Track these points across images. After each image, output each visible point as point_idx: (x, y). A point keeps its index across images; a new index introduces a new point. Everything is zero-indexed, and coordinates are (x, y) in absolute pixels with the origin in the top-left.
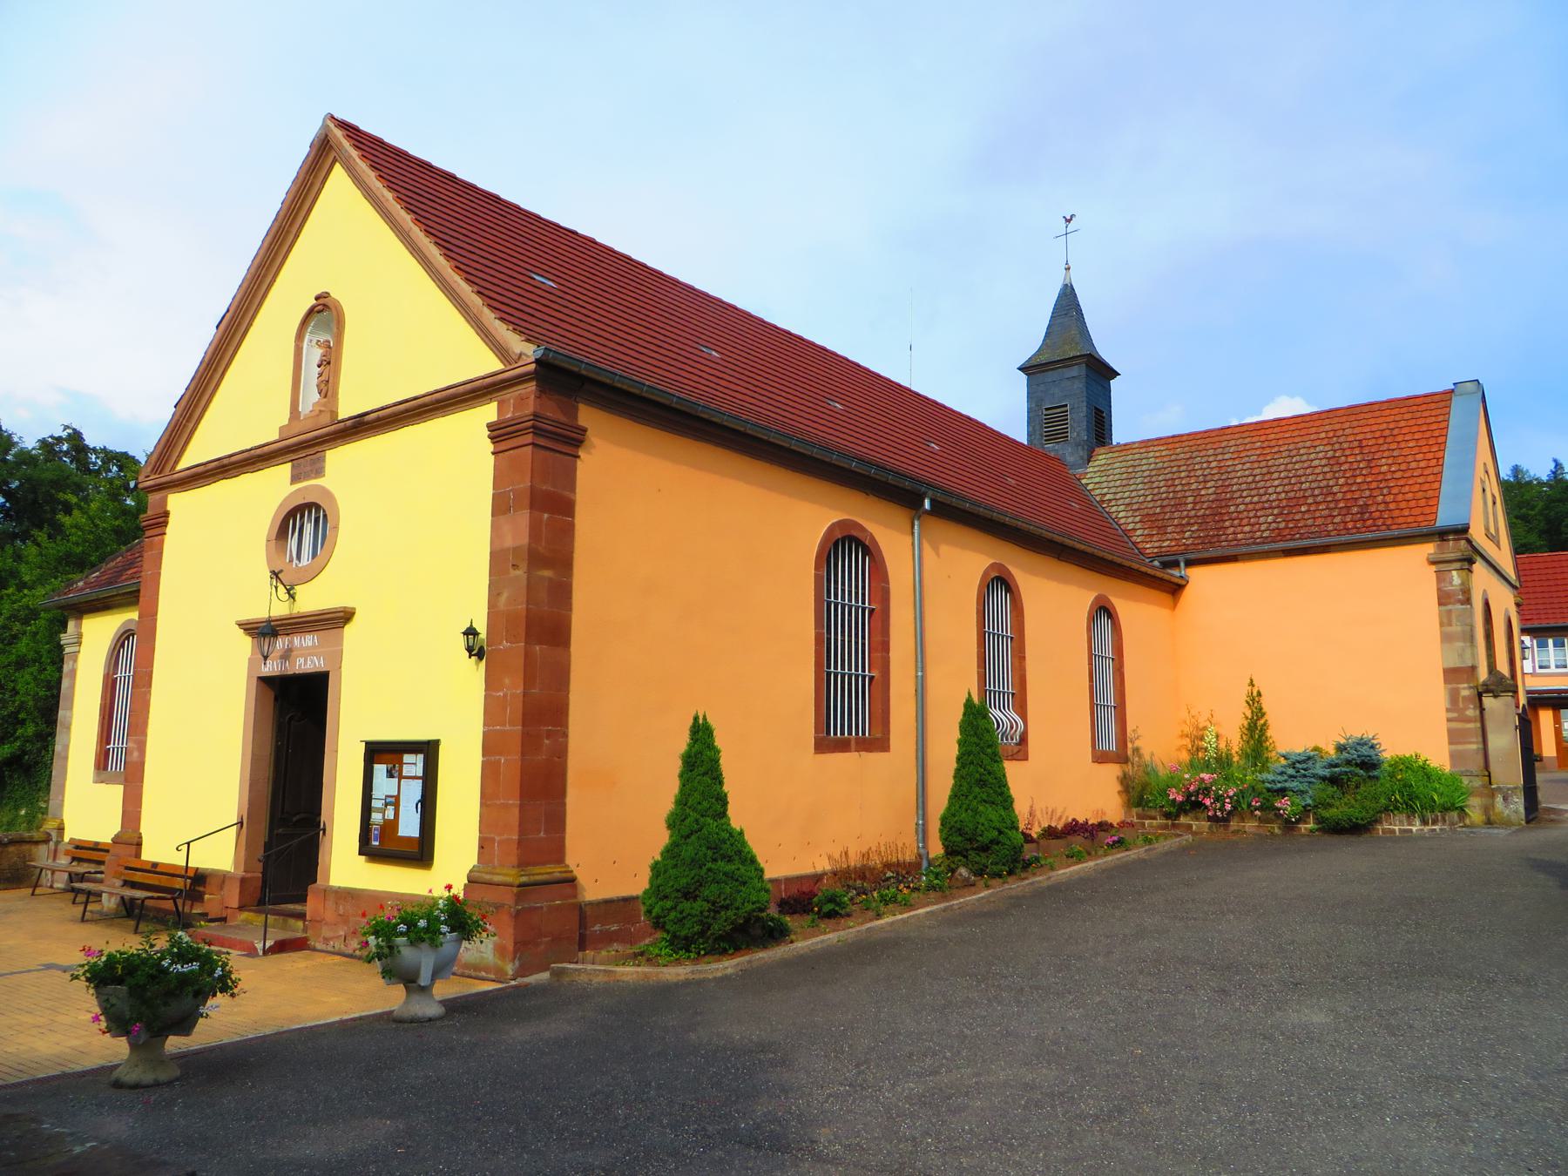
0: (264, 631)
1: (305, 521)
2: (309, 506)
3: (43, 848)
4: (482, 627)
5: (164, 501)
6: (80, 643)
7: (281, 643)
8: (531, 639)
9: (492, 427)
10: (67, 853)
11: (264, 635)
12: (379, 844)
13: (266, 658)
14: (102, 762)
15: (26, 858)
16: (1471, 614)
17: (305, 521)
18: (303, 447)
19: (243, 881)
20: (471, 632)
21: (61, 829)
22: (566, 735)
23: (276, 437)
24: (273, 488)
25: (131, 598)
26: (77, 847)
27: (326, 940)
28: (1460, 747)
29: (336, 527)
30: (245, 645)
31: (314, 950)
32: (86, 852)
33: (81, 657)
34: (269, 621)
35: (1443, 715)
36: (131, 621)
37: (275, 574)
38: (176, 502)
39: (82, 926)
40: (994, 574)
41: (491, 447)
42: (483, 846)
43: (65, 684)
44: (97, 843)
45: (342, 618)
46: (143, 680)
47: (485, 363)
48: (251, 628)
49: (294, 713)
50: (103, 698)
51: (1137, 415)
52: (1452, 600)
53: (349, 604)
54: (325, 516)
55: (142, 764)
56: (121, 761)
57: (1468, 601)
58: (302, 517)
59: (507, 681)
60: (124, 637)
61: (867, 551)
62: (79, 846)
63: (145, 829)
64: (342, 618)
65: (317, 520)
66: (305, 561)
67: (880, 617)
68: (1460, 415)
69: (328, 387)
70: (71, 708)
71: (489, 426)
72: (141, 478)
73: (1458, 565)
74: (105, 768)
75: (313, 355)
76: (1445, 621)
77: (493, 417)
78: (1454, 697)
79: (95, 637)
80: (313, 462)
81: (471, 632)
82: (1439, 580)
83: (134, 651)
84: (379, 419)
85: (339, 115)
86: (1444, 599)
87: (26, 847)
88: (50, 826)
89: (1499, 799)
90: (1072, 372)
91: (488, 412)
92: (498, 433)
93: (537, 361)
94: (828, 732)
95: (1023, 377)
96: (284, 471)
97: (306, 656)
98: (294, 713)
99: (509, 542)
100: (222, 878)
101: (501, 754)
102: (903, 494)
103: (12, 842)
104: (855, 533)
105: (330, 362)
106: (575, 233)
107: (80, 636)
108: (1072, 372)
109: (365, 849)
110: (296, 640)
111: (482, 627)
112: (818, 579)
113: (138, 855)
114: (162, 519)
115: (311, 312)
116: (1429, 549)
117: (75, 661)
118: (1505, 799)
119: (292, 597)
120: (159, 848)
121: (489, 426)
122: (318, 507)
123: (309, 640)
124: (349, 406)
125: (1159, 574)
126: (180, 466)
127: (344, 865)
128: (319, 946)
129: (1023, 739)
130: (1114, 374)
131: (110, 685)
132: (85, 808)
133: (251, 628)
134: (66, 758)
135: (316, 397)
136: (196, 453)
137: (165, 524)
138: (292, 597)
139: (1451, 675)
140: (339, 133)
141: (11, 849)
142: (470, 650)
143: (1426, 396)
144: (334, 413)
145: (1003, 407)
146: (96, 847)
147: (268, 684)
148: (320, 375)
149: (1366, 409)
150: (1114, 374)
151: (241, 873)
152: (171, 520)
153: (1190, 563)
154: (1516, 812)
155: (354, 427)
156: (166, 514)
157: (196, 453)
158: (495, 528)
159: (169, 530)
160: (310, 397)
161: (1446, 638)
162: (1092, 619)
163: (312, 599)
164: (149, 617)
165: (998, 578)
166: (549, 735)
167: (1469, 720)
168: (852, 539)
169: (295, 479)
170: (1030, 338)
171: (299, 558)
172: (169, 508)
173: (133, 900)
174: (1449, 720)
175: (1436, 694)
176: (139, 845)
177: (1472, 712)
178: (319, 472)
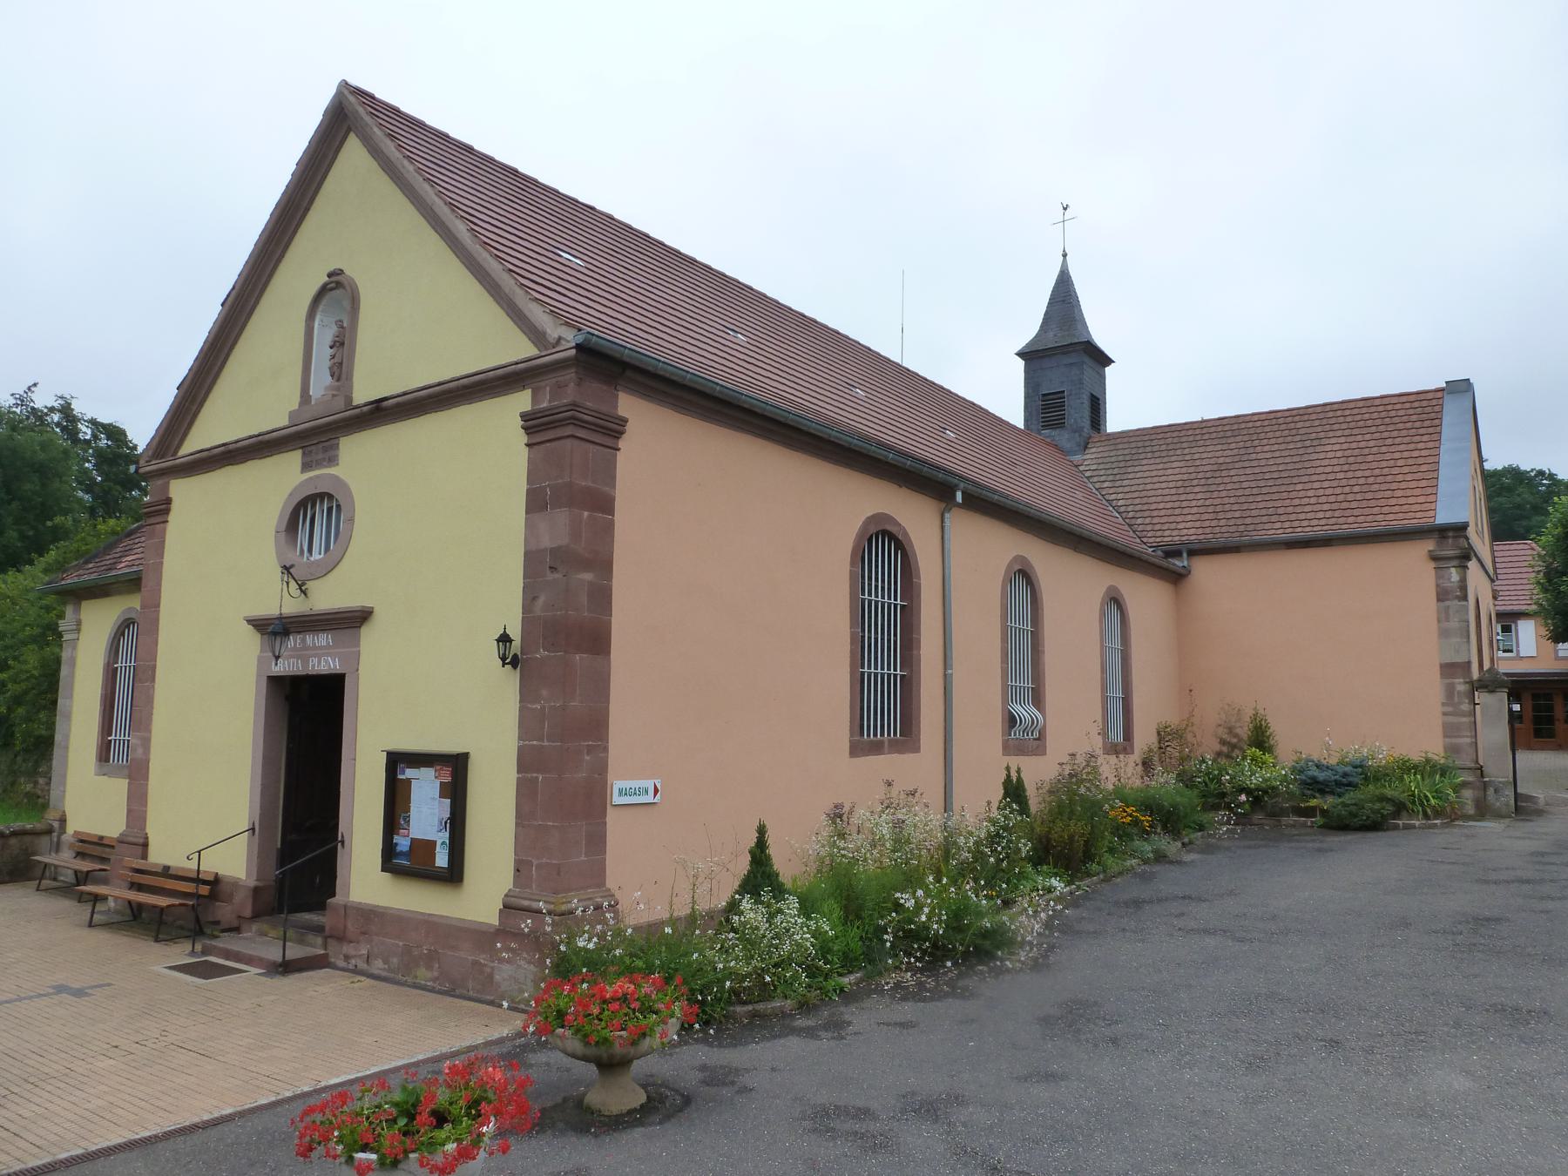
0: (275, 629)
1: (314, 513)
2: (321, 496)
3: (44, 841)
4: (515, 633)
5: (166, 488)
6: (79, 630)
7: (293, 641)
8: (562, 643)
9: (525, 417)
10: (71, 846)
11: (275, 634)
12: (405, 862)
13: (277, 658)
14: (104, 753)
15: (28, 853)
16: (1466, 608)
17: (314, 513)
18: (314, 437)
19: (256, 890)
20: (504, 639)
21: (63, 821)
22: (606, 749)
23: (285, 422)
24: (284, 476)
25: (133, 583)
26: (82, 841)
27: (347, 958)
28: (1454, 740)
29: (351, 520)
30: (252, 642)
31: (335, 967)
32: (92, 847)
33: (81, 645)
34: (281, 618)
35: (1440, 709)
36: (131, 609)
37: (287, 569)
38: (179, 489)
39: (87, 932)
40: (1017, 567)
41: (524, 438)
42: (520, 868)
43: (64, 672)
44: (102, 838)
45: (357, 619)
46: (145, 674)
47: (515, 349)
48: (260, 625)
49: (308, 717)
50: (105, 687)
51: (1131, 404)
52: (1451, 596)
53: (368, 604)
54: (338, 506)
55: (148, 762)
56: (123, 751)
57: (1465, 598)
58: (313, 506)
59: (544, 693)
60: (126, 625)
61: (900, 546)
62: (83, 840)
63: (151, 830)
64: (357, 619)
65: (330, 510)
66: (316, 556)
67: (909, 615)
68: (1452, 414)
69: (341, 371)
70: (71, 697)
71: (524, 416)
72: (142, 462)
73: (1455, 563)
74: (107, 760)
75: (324, 335)
76: (1444, 615)
77: (527, 407)
78: (1450, 691)
79: (90, 636)
80: (325, 450)
81: (504, 639)
82: (1438, 577)
83: (135, 637)
84: (398, 405)
85: (354, 82)
86: (1442, 595)
87: (27, 839)
88: (51, 816)
89: (1491, 791)
90: (1065, 360)
91: (522, 401)
92: (534, 424)
93: (578, 347)
94: (862, 734)
95: (1021, 363)
96: (294, 458)
97: (316, 656)
98: (308, 717)
99: (546, 542)
100: (235, 884)
101: (538, 771)
102: (936, 485)
103: (15, 834)
104: (889, 528)
105: (343, 344)
106: (593, 208)
107: (79, 623)
108: (1065, 360)
109: (390, 860)
110: (309, 639)
111: (515, 633)
112: (852, 575)
113: (145, 856)
114: (163, 507)
115: (323, 291)
116: (1430, 545)
117: (74, 648)
118: (1496, 791)
119: (304, 593)
120: (169, 848)
121: (524, 416)
122: (330, 497)
123: (323, 639)
124: (363, 393)
125: (1164, 563)
126: (182, 452)
127: (363, 878)
128: (341, 963)
129: (1041, 737)
130: (1108, 361)
131: (111, 675)
132: (87, 800)
133: (260, 625)
134: (66, 748)
135: (328, 380)
136: (205, 435)
137: (167, 511)
138: (304, 593)
139: (1449, 669)
140: (352, 98)
141: (13, 841)
142: (503, 659)
143: (1418, 393)
144: (349, 399)
145: (1003, 393)
146: (100, 842)
147: (277, 684)
148: (333, 357)
149: (1361, 404)
150: (1108, 361)
151: (252, 883)
152: (175, 506)
153: (1193, 553)
154: (1507, 805)
155: (371, 412)
156: (168, 501)
157: (205, 435)
158: (529, 525)
159: (172, 517)
160: (321, 382)
161: (1444, 633)
162: (1009, 580)
163: (328, 596)
164: (153, 606)
165: (1020, 571)
166: (590, 750)
167: (1463, 714)
168: (885, 533)
169: (306, 466)
170: (1028, 327)
171: (310, 551)
172: (172, 494)
173: (140, 906)
174: (1445, 714)
175: (1432, 689)
176: (145, 845)
177: (1466, 707)
178: (333, 461)
